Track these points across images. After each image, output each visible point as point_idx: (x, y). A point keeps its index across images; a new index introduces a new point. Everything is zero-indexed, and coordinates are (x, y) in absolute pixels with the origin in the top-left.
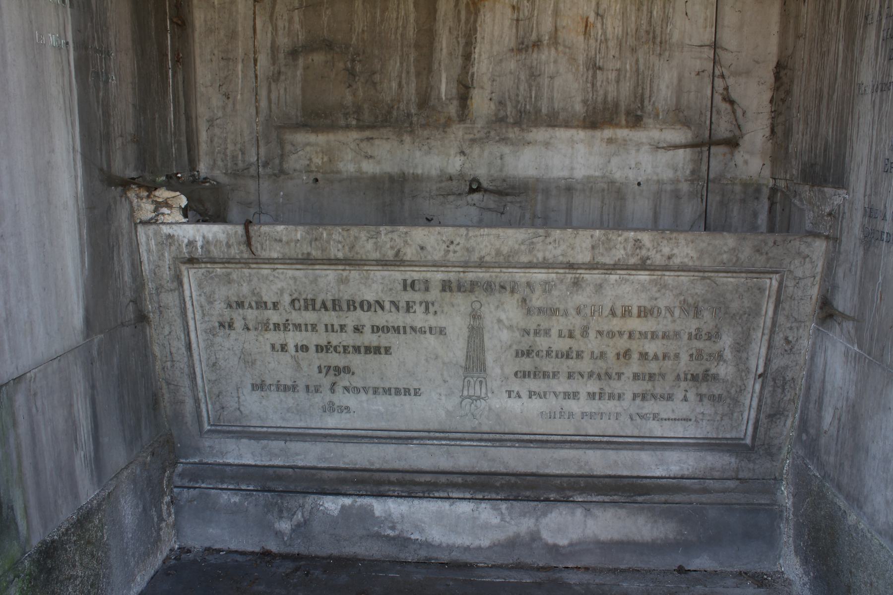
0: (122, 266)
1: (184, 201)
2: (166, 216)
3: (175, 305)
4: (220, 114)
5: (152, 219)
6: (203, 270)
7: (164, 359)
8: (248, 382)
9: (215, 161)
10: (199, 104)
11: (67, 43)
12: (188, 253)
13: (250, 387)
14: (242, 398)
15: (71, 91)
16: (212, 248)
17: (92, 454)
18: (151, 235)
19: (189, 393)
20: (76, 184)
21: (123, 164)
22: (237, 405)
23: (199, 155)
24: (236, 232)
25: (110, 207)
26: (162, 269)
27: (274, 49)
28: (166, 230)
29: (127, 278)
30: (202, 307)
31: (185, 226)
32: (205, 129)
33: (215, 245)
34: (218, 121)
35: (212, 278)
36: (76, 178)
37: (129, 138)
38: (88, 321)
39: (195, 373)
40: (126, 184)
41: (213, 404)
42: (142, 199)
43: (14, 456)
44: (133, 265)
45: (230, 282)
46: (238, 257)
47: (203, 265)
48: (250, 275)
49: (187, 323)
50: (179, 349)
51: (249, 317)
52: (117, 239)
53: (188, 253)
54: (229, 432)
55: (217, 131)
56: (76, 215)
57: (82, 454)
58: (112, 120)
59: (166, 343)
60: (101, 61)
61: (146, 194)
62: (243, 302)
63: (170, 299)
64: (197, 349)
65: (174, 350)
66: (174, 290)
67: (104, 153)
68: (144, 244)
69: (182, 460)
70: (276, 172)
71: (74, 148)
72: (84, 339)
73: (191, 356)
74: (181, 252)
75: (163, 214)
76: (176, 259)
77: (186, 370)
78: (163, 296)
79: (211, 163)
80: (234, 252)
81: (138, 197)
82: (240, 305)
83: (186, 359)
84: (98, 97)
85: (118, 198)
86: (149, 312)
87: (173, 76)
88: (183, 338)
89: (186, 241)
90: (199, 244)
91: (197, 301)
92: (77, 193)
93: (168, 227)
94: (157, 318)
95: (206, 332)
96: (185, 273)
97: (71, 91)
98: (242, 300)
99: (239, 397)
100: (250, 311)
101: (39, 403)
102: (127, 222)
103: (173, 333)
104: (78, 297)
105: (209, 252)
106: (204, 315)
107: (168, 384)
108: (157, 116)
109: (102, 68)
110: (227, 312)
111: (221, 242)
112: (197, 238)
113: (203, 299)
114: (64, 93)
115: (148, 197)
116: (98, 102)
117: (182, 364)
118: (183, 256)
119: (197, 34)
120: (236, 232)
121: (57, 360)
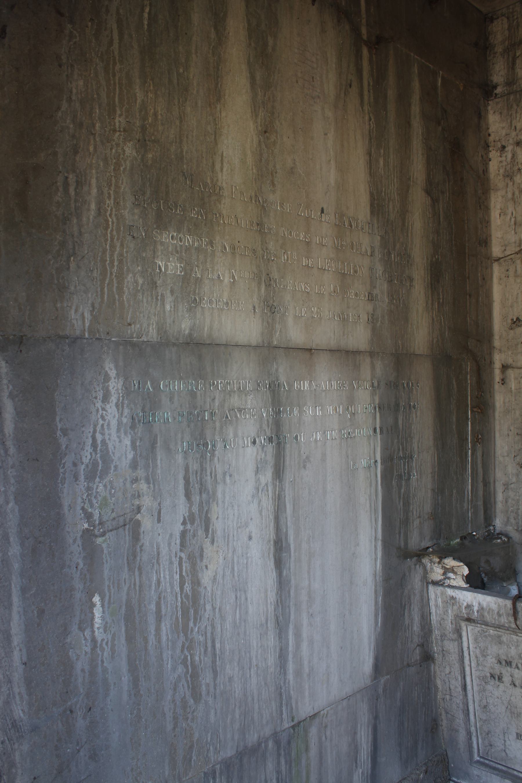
0: (412, 620)
1: (466, 571)
2: (452, 580)
3: (454, 652)
4: (514, 480)
5: (440, 581)
6: (479, 629)
7: (444, 692)
8: (513, 731)
9: (508, 518)
10: (497, 470)
11: (376, 461)
12: (467, 614)
13: (515, 735)
14: (508, 743)
15: (376, 496)
16: (486, 614)
17: (369, 772)
18: (439, 594)
19: (463, 725)
20: (376, 564)
21: (418, 537)
22: (503, 747)
23: (495, 512)
24: (506, 605)
25: (405, 575)
26: (446, 622)
28: (450, 592)
29: (416, 628)
30: (477, 657)
31: (465, 592)
32: (502, 491)
33: (488, 612)
34: (512, 486)
35: (485, 636)
36: (376, 560)
37: (426, 517)
38: (377, 669)
39: (468, 710)
40: (421, 554)
41: (483, 739)
42: (434, 564)
43: (304, 774)
44: (422, 616)
45: (500, 643)
46: (506, 625)
47: (479, 625)
48: (518, 641)
49: (464, 668)
50: (456, 687)
51: (516, 676)
52: (409, 598)
53: (467, 614)
54: (495, 769)
55: (511, 494)
56: (373, 587)
57: (361, 771)
58: (411, 507)
59: (447, 680)
60: (404, 465)
61: (437, 560)
62: (510, 662)
63: (451, 647)
64: (471, 691)
65: (452, 687)
66: (455, 640)
67: (402, 535)
68: (433, 599)
69: (454, 779)
71: (376, 538)
72: (372, 681)
73: (466, 695)
74: (461, 612)
75: (449, 578)
76: (458, 618)
77: (461, 705)
78: (446, 643)
79: (505, 520)
80: (504, 620)
81: (431, 561)
82: (509, 663)
83: (461, 697)
84: (400, 493)
85: (413, 567)
86: (434, 652)
87: (472, 454)
88: (460, 679)
89: (465, 604)
90: (476, 608)
91: (474, 652)
92: (376, 571)
93: (452, 590)
94: (441, 658)
95: (479, 678)
96: (464, 628)
97: (376, 496)
98: (511, 660)
99: (505, 741)
100: (517, 670)
101: (328, 733)
102: (420, 583)
103: (452, 674)
104: (370, 650)
105: (483, 616)
106: (478, 665)
107: (447, 713)
108: (455, 491)
109: (405, 469)
110: (497, 667)
111: (493, 611)
112: (474, 604)
113: (478, 651)
114: (370, 500)
115: (439, 563)
116: (400, 497)
117: (458, 699)
118: (462, 615)
119: (497, 414)
120: (506, 605)
121: (347, 699)
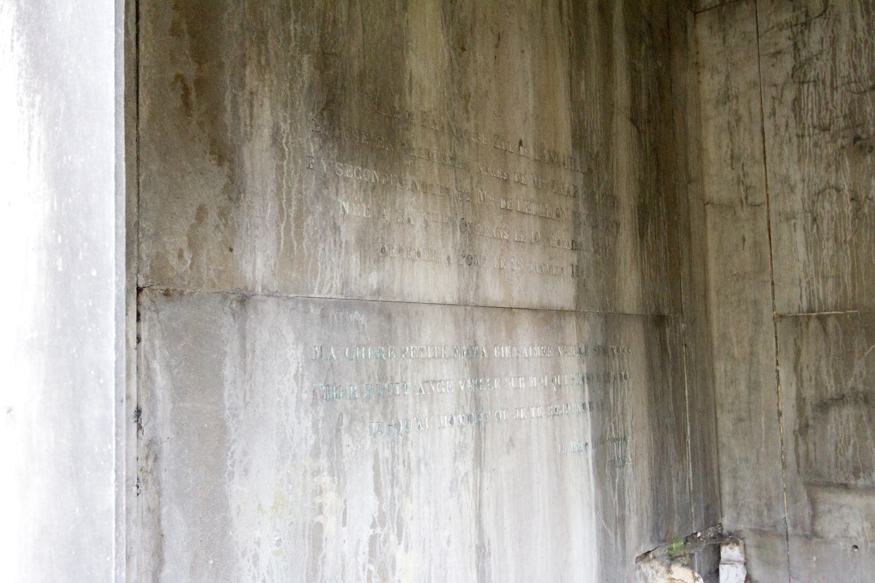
27: (801, 401)
67: (618, 536)
70: (808, 533)
